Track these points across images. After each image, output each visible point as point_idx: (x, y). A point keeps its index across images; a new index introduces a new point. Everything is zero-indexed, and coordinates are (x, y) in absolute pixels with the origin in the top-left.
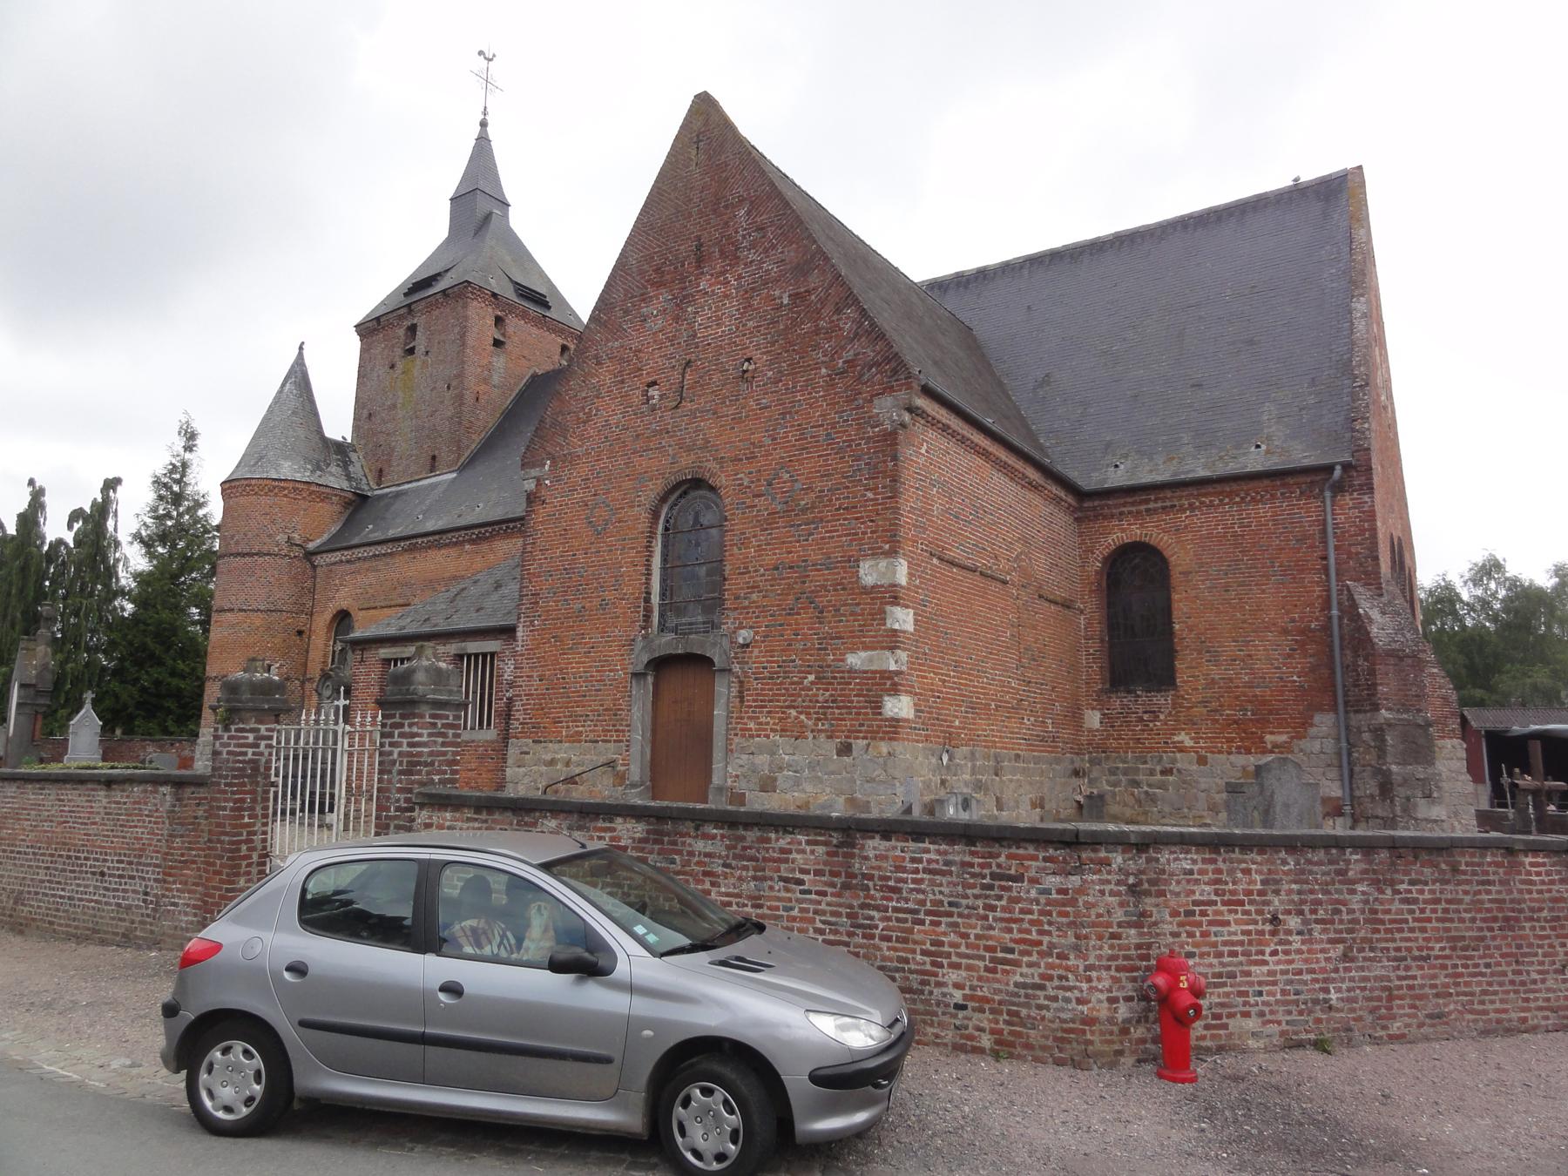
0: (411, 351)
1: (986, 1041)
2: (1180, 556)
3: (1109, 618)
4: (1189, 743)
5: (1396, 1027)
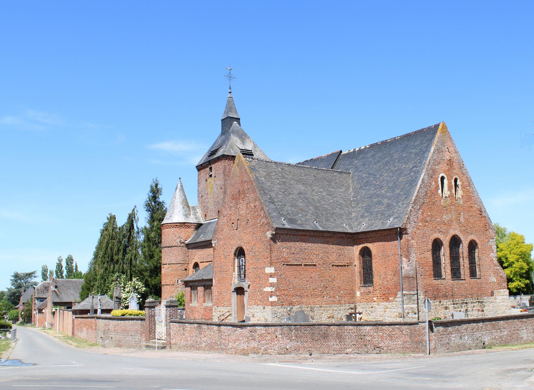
0: (211, 176)
1: (234, 353)
2: (374, 252)
3: (363, 266)
4: (376, 300)
5: (300, 352)
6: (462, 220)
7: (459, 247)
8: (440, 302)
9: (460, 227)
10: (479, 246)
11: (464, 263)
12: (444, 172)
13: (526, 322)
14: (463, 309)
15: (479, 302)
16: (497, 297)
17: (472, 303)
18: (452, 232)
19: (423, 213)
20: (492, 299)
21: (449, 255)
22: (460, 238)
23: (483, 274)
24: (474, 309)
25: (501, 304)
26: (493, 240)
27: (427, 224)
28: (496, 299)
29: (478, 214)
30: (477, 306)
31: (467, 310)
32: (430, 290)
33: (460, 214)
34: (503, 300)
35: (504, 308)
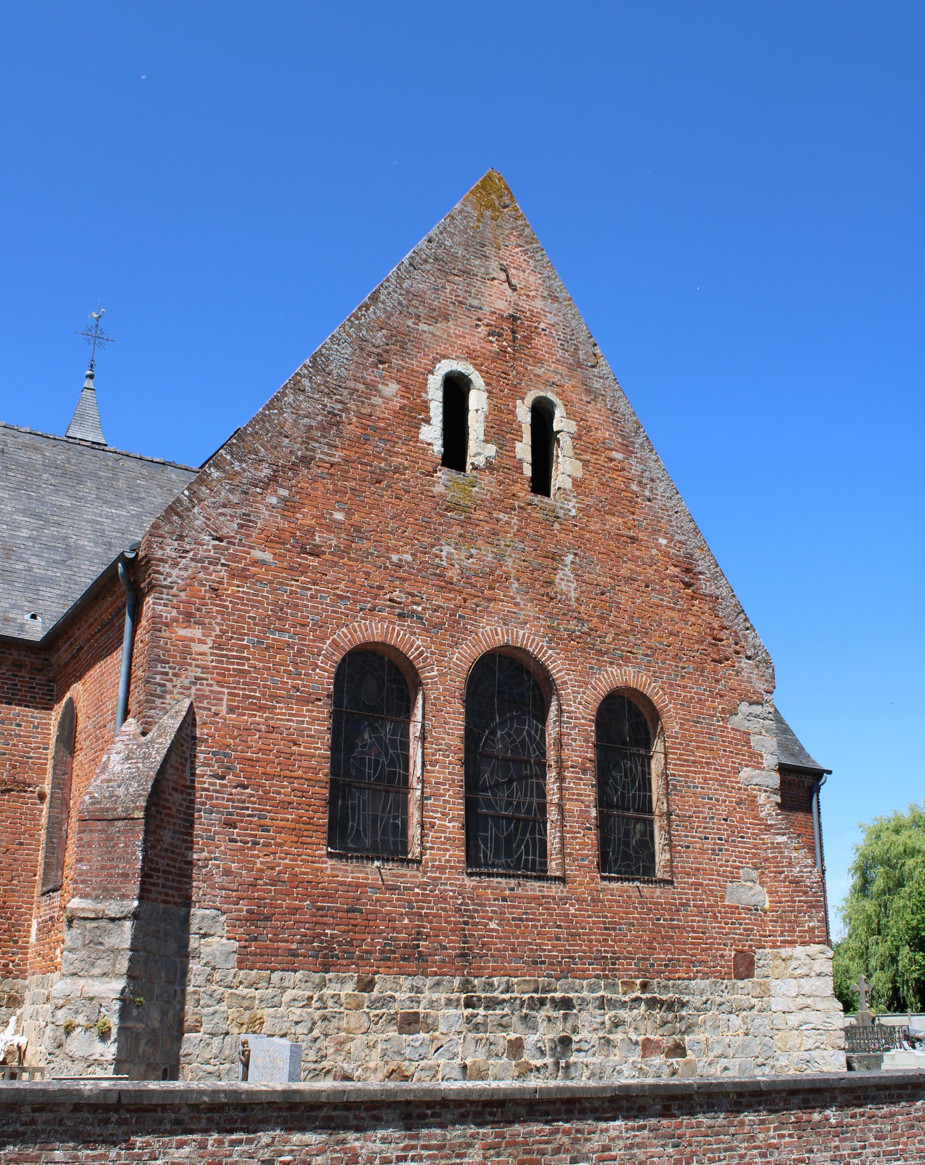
6: (565, 582)
7: (543, 719)
8: (366, 986)
9: (551, 616)
10: (672, 723)
11: (571, 800)
12: (470, 356)
13: (840, 1130)
14: (545, 1033)
15: (652, 1003)
16: (773, 983)
17: (602, 1004)
18: (490, 633)
19: (289, 507)
20: (743, 991)
21: (458, 743)
22: (543, 668)
23: (686, 861)
24: (617, 1037)
25: (793, 1020)
26: (757, 709)
27: (313, 562)
28: (765, 992)
29: (673, 578)
30: (640, 1024)
31: (565, 1042)
32: (294, 910)
33: (555, 557)
34: (801, 1001)
35: (809, 1043)
